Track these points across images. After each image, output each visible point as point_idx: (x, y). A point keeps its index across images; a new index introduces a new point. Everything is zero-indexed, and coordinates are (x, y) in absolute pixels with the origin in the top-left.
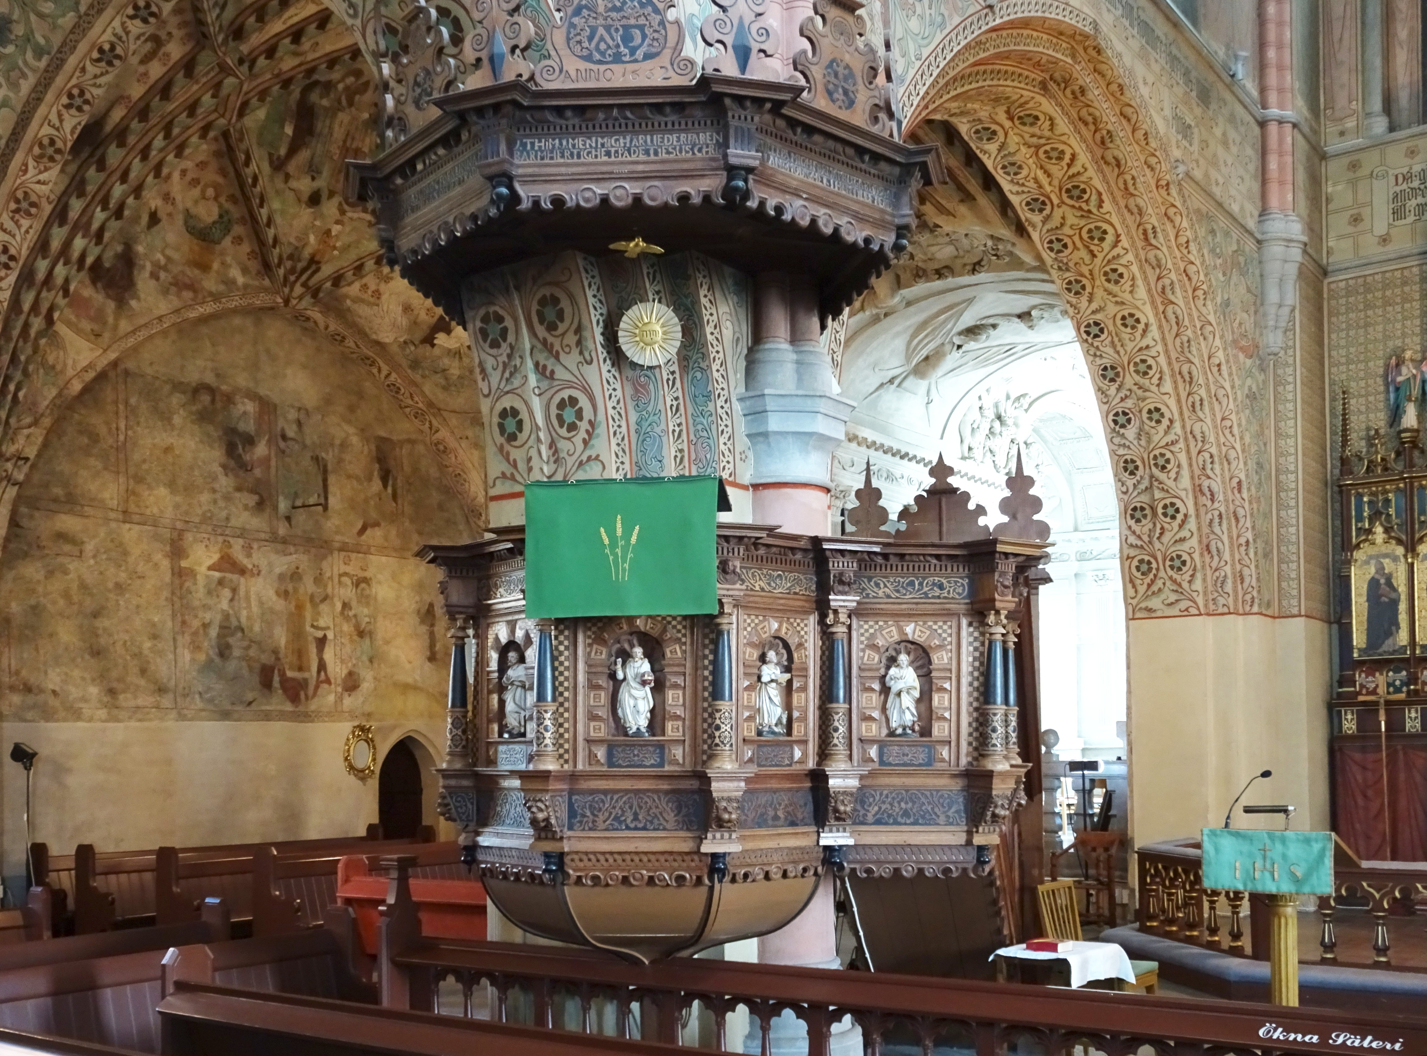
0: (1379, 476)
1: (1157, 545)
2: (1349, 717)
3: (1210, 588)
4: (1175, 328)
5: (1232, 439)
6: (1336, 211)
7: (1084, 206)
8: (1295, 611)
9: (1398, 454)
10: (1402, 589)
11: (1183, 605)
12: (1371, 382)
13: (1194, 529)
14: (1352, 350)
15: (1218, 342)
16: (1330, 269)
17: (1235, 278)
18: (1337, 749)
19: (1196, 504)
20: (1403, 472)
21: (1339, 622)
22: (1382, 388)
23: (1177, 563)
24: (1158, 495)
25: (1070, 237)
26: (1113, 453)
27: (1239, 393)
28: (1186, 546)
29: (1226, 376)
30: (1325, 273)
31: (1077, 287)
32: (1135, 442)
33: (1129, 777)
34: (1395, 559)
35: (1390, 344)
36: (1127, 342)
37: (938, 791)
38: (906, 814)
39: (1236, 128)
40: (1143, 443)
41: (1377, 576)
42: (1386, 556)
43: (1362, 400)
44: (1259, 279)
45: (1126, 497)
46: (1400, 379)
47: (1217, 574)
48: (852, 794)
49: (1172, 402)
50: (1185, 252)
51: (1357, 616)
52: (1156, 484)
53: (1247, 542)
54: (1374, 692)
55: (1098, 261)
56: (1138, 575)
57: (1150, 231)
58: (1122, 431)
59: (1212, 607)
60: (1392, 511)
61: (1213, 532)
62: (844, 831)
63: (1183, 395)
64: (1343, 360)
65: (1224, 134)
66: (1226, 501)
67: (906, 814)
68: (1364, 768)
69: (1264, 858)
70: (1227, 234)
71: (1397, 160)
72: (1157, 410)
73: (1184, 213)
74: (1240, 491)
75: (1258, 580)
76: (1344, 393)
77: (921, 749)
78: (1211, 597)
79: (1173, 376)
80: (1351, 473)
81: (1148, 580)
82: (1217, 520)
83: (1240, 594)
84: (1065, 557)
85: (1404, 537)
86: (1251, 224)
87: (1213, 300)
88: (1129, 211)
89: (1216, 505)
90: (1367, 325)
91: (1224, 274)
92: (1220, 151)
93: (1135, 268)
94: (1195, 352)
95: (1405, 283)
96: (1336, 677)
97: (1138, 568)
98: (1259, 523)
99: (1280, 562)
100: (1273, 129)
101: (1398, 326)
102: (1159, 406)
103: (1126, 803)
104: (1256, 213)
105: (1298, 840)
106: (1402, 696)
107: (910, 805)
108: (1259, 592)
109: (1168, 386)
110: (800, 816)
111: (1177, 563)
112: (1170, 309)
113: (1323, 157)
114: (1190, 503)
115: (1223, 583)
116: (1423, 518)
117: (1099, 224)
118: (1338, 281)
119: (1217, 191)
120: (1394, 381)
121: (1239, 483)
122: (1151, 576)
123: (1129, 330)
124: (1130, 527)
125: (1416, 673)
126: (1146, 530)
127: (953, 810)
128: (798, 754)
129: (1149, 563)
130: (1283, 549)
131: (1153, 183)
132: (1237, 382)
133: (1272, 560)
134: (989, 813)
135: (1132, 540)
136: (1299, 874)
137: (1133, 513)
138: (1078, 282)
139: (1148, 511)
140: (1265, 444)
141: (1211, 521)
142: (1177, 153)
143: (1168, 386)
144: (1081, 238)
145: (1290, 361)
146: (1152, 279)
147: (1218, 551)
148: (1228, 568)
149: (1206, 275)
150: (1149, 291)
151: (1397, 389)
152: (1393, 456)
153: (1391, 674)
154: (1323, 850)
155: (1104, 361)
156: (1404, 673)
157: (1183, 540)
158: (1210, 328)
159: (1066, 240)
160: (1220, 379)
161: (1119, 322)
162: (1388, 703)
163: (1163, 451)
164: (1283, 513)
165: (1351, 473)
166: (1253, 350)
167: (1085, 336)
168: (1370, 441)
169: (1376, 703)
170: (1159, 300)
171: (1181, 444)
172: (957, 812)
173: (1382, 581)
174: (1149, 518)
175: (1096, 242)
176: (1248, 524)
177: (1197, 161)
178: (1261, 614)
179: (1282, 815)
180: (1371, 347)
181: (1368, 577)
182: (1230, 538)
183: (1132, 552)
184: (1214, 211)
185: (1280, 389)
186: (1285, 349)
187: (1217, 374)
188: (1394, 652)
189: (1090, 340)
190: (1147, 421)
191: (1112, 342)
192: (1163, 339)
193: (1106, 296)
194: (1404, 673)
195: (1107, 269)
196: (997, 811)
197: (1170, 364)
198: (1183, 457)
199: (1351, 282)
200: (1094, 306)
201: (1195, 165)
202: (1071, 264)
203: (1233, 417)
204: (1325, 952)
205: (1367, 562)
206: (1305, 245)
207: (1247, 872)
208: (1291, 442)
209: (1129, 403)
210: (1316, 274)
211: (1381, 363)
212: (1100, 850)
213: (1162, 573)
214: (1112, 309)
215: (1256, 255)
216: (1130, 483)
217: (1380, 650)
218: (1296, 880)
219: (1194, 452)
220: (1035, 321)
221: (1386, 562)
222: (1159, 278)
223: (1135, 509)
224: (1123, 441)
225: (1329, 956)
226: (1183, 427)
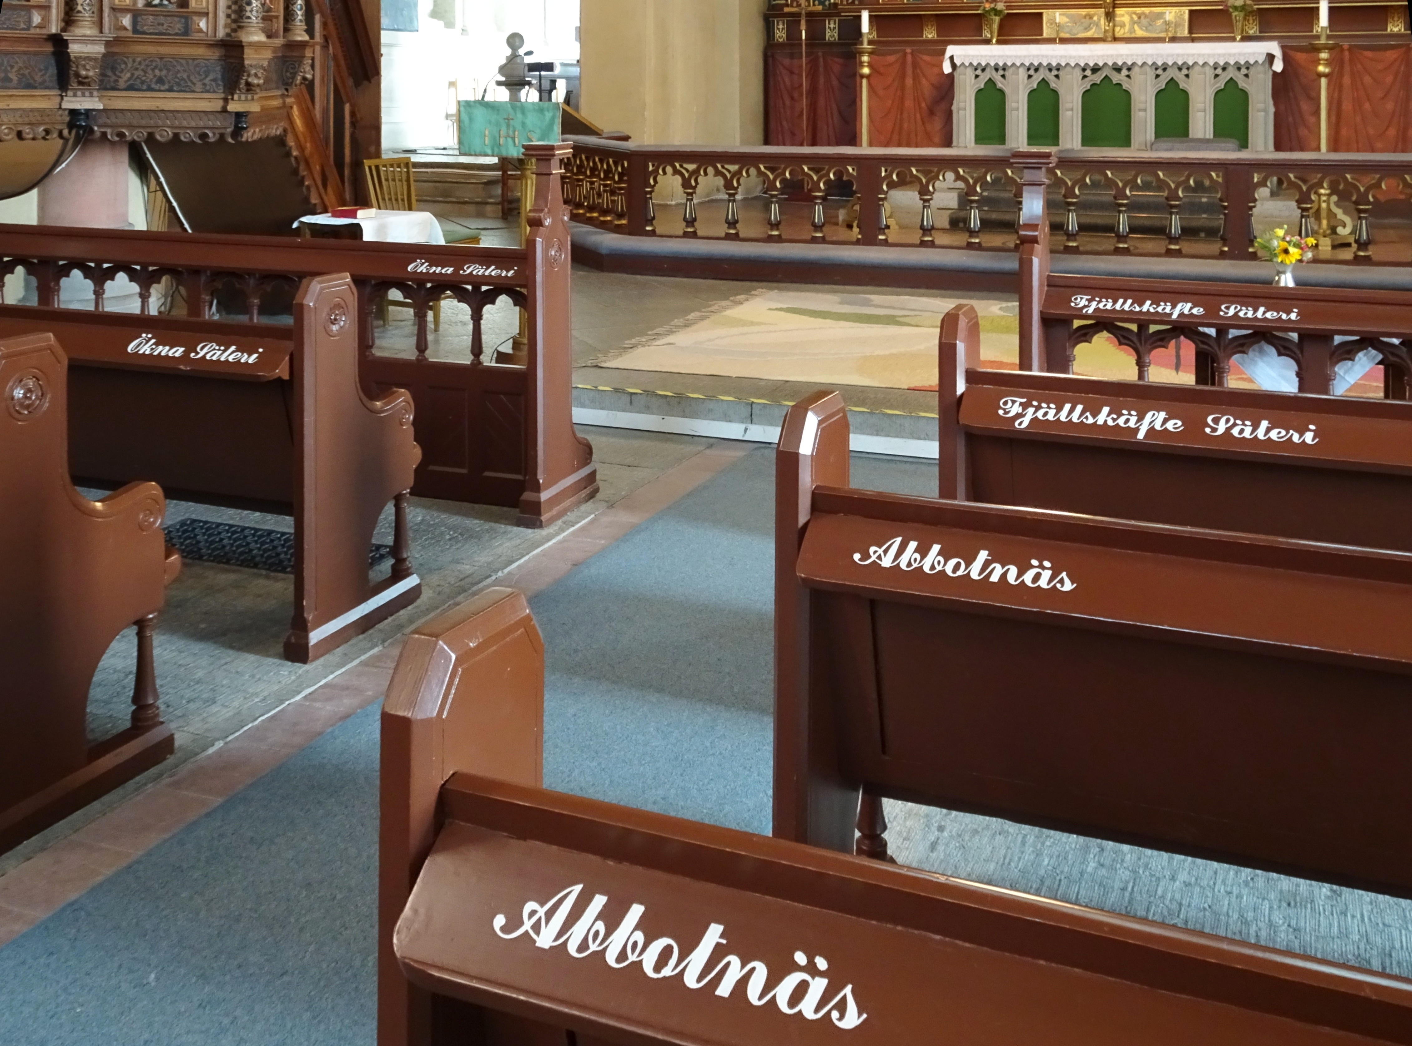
2: (781, 27)
37: (194, 59)
38: (160, 81)
48: (95, 59)
62: (91, 96)
67: (160, 81)
68: (792, 73)
69: (508, 126)
77: (176, 19)
107: (164, 72)
110: (38, 78)
127: (210, 77)
128: (37, 19)
134: (243, 82)
154: (553, 119)
162: (810, 15)
169: (798, 15)
172: (215, 80)
196: (250, 80)
207: (494, 138)
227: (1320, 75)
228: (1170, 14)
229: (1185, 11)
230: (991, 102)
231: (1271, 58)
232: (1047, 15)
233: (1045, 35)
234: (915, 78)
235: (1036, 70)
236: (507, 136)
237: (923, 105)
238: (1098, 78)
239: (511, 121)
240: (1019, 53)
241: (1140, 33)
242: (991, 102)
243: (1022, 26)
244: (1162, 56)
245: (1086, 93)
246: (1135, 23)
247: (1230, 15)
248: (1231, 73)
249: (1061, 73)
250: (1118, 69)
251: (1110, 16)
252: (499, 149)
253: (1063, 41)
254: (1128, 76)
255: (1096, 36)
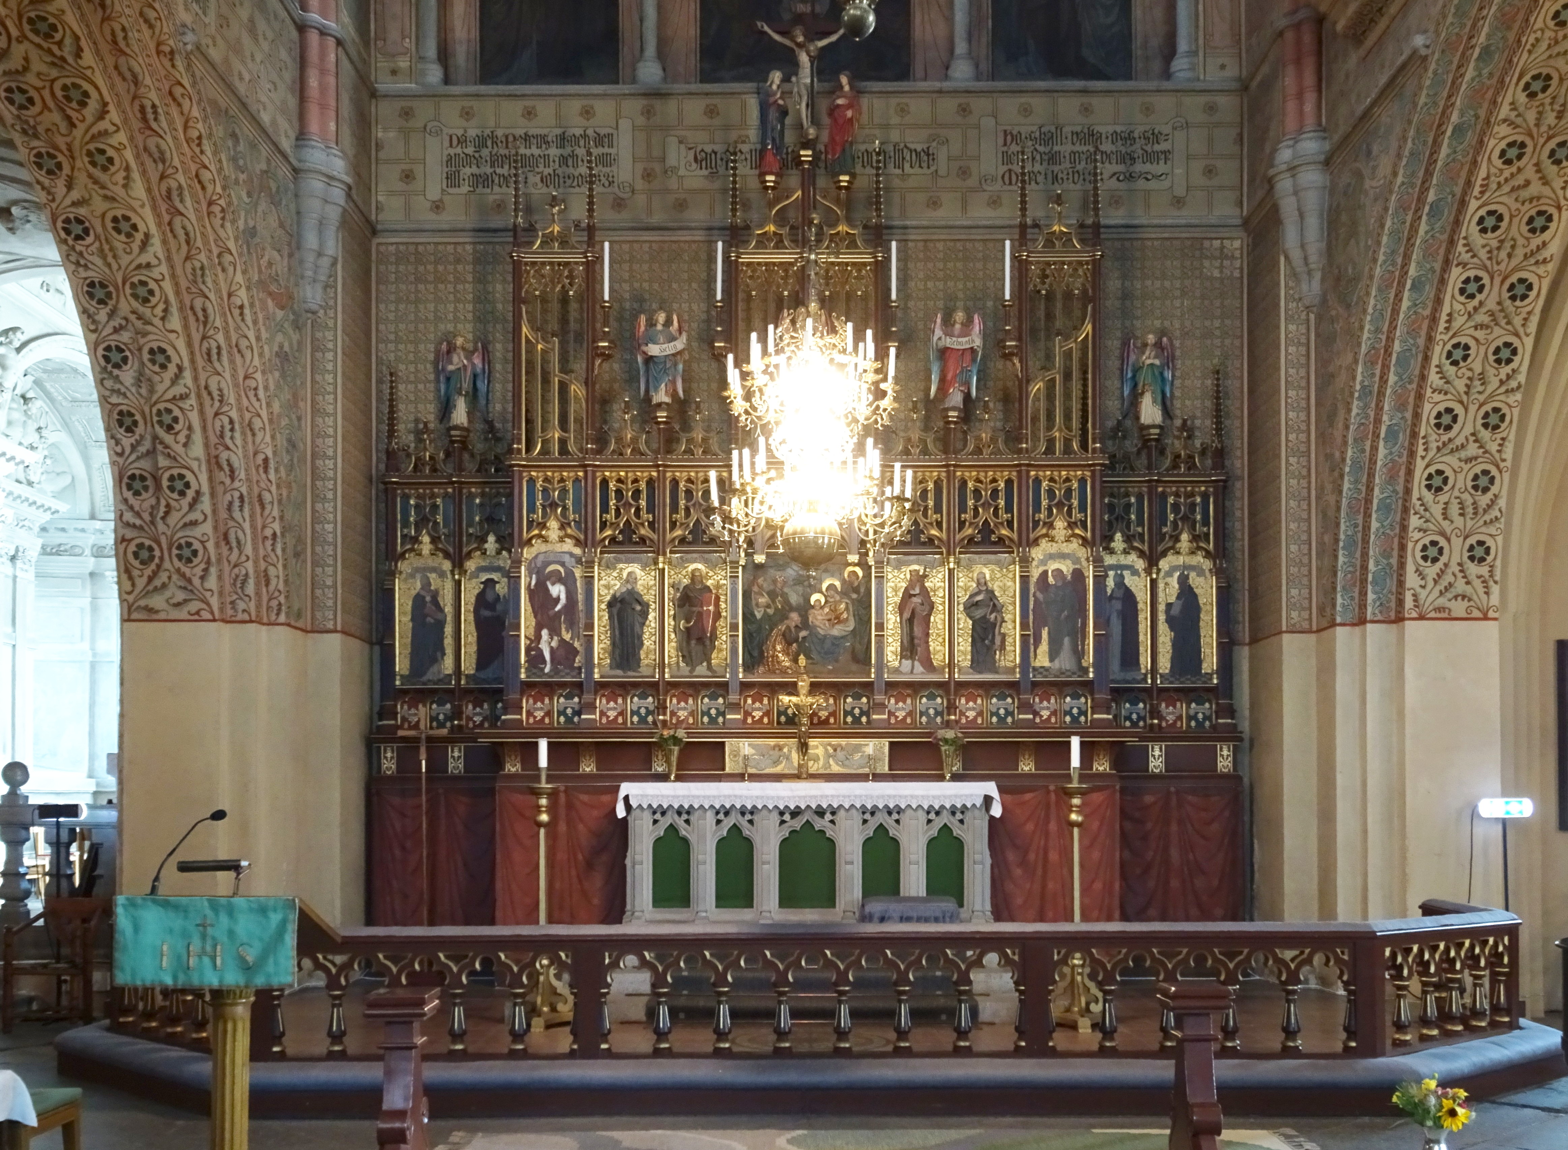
0: (426, 477)
1: (161, 527)
2: (389, 755)
3: (228, 588)
4: (185, 248)
5: (257, 405)
6: (387, 161)
7: (55, 49)
8: (330, 625)
9: (448, 454)
10: (448, 609)
11: (194, 606)
12: (421, 367)
13: (208, 510)
14: (402, 326)
15: (239, 278)
16: (379, 227)
17: (263, 206)
18: (375, 792)
19: (211, 479)
20: (452, 476)
21: (380, 643)
22: (432, 377)
23: (187, 552)
24: (163, 462)
25: (37, 89)
26: (104, 400)
27: (266, 348)
28: (198, 532)
29: (250, 324)
30: (374, 232)
31: (50, 164)
32: (133, 390)
33: (119, 826)
34: (442, 575)
35: (442, 327)
36: (120, 252)
39: (268, 20)
40: (144, 391)
41: (423, 593)
42: (433, 570)
43: (411, 387)
44: (295, 217)
45: (121, 460)
46: (451, 368)
47: (236, 570)
49: (181, 344)
50: (197, 150)
51: (401, 637)
52: (160, 447)
53: (274, 534)
54: (416, 727)
55: (78, 133)
56: (136, 563)
57: (149, 110)
58: (116, 372)
59: (230, 612)
60: (439, 518)
61: (232, 518)
63: (196, 337)
64: (392, 337)
65: (251, 20)
66: (248, 480)
69: (204, 937)
70: (253, 146)
71: (450, 113)
72: (162, 351)
73: (195, 98)
74: (266, 471)
75: (286, 582)
76: (391, 374)
78: (229, 599)
79: (181, 309)
80: (398, 470)
81: (148, 572)
82: (237, 503)
83: (265, 599)
84: (77, 551)
85: (451, 550)
86: (286, 144)
87: (234, 221)
88: (120, 74)
89: (237, 484)
90: (417, 301)
91: (249, 195)
92: (247, 41)
93: (129, 155)
94: (210, 285)
95: (458, 261)
96: (376, 709)
97: (136, 555)
98: (288, 516)
99: (315, 564)
100: (313, 37)
101: (451, 307)
102: (164, 345)
103: (114, 859)
104: (293, 135)
105: (251, 910)
106: (444, 732)
108: (287, 597)
109: (175, 322)
111: (187, 552)
112: (178, 221)
113: (374, 94)
114: (204, 477)
115: (244, 582)
116: (471, 531)
117: (78, 81)
118: (387, 243)
119: (242, 89)
120: (444, 369)
121: (266, 460)
122: (153, 566)
123: (122, 238)
124: (126, 501)
125: (460, 706)
126: (146, 505)
129: (151, 549)
130: (318, 549)
131: (152, 46)
132: (264, 335)
133: (305, 561)
135: (128, 516)
136: (250, 959)
137: (129, 482)
138: (52, 156)
139: (149, 482)
140: (299, 419)
141: (231, 503)
142: (186, 17)
143: (175, 322)
144: (53, 94)
145: (331, 323)
146: (154, 177)
147: (238, 542)
148: (250, 565)
149: (224, 188)
150: (149, 190)
151: (448, 379)
152: (442, 455)
153: (434, 706)
154: (284, 922)
155: (90, 274)
156: (448, 706)
157: (194, 523)
158: (231, 258)
159: (32, 93)
160: (242, 325)
161: (110, 225)
162: (430, 739)
163: (169, 406)
164: (319, 506)
165: (398, 470)
166: (285, 300)
167: (63, 234)
168: (418, 434)
169: (417, 740)
170: (163, 207)
171: (193, 401)
173: (428, 599)
174: (151, 491)
175: (74, 105)
176: (276, 513)
177: (213, 38)
178: (289, 625)
179: (232, 874)
180: (421, 326)
181: (414, 593)
182: (253, 527)
183: (129, 534)
184: (234, 109)
185: (319, 355)
186: (326, 307)
187: (238, 319)
188: (440, 681)
189: (71, 242)
190: (149, 365)
191: (101, 250)
192: (169, 259)
193: (90, 186)
194: (448, 706)
195: (92, 147)
197: (177, 293)
198: (194, 418)
199: (401, 248)
200: (75, 195)
201: (210, 42)
202: (41, 129)
203: (258, 376)
204: (333, 1043)
205: (412, 576)
206: (350, 188)
207: (179, 957)
208: (330, 421)
209: (125, 337)
210: (362, 229)
211: (432, 347)
212: (78, 922)
213: (167, 565)
214: (99, 205)
215: (292, 186)
216: (127, 442)
217: (425, 679)
218: (247, 968)
219: (210, 412)
220: (18, 223)
221: (433, 576)
222: (162, 177)
223: (132, 477)
224: (117, 386)
225: (337, 1048)
226: (196, 379)
227: (1073, 824)
228: (870, 746)
229: (885, 743)
230: (673, 852)
231: (988, 800)
232: (730, 744)
233: (728, 770)
234: (569, 823)
235: (727, 814)
236: (203, 953)
237: (580, 857)
238: (797, 824)
239: (209, 929)
240: (708, 793)
241: (836, 769)
242: (673, 852)
243: (702, 758)
244: (872, 797)
245: (784, 842)
246: (830, 756)
247: (939, 750)
248: (945, 818)
249: (756, 818)
250: (820, 812)
251: (803, 747)
252: (185, 974)
253: (754, 778)
254: (832, 822)
255: (787, 771)
